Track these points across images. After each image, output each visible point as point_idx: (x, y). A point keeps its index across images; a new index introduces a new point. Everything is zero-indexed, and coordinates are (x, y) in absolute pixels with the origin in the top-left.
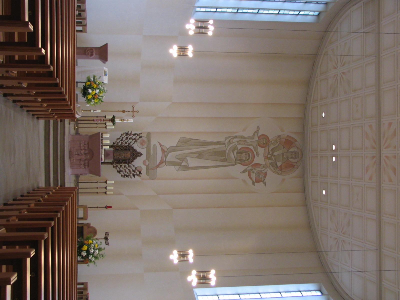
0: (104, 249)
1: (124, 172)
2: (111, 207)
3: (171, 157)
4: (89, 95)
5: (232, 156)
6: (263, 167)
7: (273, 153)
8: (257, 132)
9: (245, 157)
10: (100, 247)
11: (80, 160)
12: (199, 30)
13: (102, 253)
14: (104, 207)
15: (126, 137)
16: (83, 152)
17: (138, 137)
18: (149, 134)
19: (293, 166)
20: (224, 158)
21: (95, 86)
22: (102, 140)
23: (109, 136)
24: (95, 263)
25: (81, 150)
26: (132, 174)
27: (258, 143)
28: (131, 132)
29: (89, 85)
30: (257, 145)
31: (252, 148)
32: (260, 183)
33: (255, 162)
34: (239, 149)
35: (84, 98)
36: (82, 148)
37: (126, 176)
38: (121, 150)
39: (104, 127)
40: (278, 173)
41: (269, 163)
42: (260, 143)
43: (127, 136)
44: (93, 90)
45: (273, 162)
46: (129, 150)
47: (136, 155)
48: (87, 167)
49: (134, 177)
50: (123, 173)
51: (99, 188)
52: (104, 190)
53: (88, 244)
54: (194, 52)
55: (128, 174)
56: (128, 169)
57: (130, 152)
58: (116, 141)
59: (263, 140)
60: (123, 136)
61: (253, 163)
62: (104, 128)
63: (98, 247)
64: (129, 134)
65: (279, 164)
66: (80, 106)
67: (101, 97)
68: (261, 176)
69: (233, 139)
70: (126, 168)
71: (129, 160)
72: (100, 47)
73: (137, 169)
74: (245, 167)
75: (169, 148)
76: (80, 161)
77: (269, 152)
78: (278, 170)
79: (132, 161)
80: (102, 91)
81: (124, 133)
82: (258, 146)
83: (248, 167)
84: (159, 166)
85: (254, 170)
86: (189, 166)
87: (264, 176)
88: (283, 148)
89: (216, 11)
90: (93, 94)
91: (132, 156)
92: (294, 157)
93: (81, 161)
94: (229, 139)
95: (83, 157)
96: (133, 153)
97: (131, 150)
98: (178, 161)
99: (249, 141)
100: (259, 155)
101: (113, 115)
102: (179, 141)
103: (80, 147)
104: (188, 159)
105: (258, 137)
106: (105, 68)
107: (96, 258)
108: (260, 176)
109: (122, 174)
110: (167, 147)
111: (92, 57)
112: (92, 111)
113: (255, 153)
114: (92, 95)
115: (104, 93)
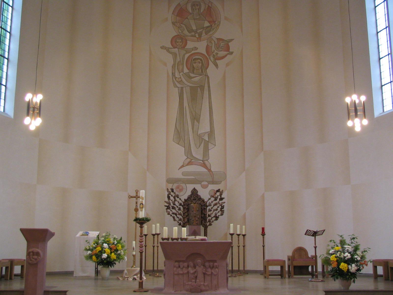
0: (341, 236)
1: (217, 212)
2: (263, 229)
3: (198, 154)
4: (111, 258)
5: (197, 79)
6: (211, 42)
7: (193, 31)
8: (168, 50)
9: (198, 64)
10: (338, 242)
11: (204, 274)
12: (31, 112)
13: (350, 239)
14: (263, 238)
15: (171, 209)
16: (191, 271)
17: (172, 193)
18: (169, 181)
19: (209, 8)
20: (199, 89)
21: (99, 249)
22: (173, 239)
23: (167, 228)
24: (365, 251)
25: (188, 272)
26: (219, 201)
27: (181, 48)
28: (165, 202)
29: (97, 258)
30: (184, 49)
31: (187, 56)
32: (230, 46)
33: (204, 52)
34: (188, 71)
35: (115, 264)
36: (185, 271)
37: (223, 210)
38: (188, 215)
39: (158, 237)
40: (217, 26)
41: (206, 36)
42: (181, 46)
43: (170, 207)
44: (104, 252)
45: (204, 31)
46: (188, 205)
47: (195, 197)
48: (215, 264)
49: (224, 198)
50: (219, 213)
51: (239, 244)
52: (241, 237)
53: (337, 261)
54: (35, 93)
55: (220, 207)
56: (213, 206)
57: (191, 203)
58: (177, 221)
59: (178, 42)
60: (171, 213)
61: (206, 55)
62: (159, 237)
63: (339, 245)
64: (168, 205)
65: (207, 24)
66: (127, 270)
67: (114, 241)
68: (221, 45)
69: (176, 78)
70: (212, 210)
71: (202, 206)
72: (27, 240)
73: (213, 195)
74: (211, 65)
75: (186, 156)
76: (206, 274)
77: (192, 36)
78: (214, 25)
79: (203, 201)
80: (107, 240)
81: (167, 212)
82: (185, 48)
83: (211, 60)
84: (209, 169)
85: (214, 54)
86: (209, 132)
87: (221, 42)
88: (188, 19)
89: (6, 86)
90: (110, 252)
91: (196, 202)
92: (198, 7)
93: (207, 273)
94: (176, 83)
95: (200, 269)
96: (193, 199)
97: (188, 202)
98: (202, 145)
99: (178, 59)
100: (196, 47)
101: (133, 221)
102: (178, 144)
103: (183, 274)
104: (200, 132)
105: (174, 48)
106: (78, 235)
107: (356, 249)
108: (222, 46)
109: (219, 214)
110: (185, 159)
111: (41, 253)
112: (134, 253)
113: (193, 52)
114: (111, 253)
115: (110, 237)
